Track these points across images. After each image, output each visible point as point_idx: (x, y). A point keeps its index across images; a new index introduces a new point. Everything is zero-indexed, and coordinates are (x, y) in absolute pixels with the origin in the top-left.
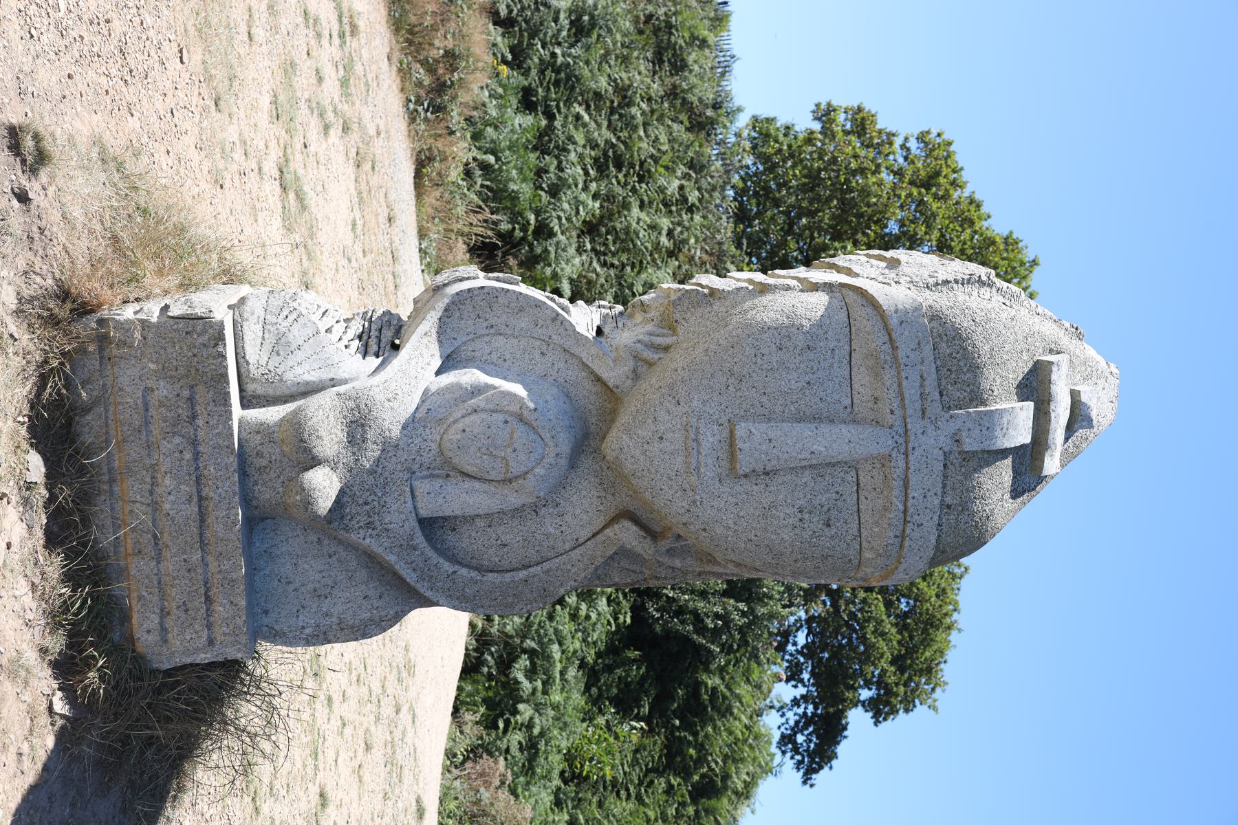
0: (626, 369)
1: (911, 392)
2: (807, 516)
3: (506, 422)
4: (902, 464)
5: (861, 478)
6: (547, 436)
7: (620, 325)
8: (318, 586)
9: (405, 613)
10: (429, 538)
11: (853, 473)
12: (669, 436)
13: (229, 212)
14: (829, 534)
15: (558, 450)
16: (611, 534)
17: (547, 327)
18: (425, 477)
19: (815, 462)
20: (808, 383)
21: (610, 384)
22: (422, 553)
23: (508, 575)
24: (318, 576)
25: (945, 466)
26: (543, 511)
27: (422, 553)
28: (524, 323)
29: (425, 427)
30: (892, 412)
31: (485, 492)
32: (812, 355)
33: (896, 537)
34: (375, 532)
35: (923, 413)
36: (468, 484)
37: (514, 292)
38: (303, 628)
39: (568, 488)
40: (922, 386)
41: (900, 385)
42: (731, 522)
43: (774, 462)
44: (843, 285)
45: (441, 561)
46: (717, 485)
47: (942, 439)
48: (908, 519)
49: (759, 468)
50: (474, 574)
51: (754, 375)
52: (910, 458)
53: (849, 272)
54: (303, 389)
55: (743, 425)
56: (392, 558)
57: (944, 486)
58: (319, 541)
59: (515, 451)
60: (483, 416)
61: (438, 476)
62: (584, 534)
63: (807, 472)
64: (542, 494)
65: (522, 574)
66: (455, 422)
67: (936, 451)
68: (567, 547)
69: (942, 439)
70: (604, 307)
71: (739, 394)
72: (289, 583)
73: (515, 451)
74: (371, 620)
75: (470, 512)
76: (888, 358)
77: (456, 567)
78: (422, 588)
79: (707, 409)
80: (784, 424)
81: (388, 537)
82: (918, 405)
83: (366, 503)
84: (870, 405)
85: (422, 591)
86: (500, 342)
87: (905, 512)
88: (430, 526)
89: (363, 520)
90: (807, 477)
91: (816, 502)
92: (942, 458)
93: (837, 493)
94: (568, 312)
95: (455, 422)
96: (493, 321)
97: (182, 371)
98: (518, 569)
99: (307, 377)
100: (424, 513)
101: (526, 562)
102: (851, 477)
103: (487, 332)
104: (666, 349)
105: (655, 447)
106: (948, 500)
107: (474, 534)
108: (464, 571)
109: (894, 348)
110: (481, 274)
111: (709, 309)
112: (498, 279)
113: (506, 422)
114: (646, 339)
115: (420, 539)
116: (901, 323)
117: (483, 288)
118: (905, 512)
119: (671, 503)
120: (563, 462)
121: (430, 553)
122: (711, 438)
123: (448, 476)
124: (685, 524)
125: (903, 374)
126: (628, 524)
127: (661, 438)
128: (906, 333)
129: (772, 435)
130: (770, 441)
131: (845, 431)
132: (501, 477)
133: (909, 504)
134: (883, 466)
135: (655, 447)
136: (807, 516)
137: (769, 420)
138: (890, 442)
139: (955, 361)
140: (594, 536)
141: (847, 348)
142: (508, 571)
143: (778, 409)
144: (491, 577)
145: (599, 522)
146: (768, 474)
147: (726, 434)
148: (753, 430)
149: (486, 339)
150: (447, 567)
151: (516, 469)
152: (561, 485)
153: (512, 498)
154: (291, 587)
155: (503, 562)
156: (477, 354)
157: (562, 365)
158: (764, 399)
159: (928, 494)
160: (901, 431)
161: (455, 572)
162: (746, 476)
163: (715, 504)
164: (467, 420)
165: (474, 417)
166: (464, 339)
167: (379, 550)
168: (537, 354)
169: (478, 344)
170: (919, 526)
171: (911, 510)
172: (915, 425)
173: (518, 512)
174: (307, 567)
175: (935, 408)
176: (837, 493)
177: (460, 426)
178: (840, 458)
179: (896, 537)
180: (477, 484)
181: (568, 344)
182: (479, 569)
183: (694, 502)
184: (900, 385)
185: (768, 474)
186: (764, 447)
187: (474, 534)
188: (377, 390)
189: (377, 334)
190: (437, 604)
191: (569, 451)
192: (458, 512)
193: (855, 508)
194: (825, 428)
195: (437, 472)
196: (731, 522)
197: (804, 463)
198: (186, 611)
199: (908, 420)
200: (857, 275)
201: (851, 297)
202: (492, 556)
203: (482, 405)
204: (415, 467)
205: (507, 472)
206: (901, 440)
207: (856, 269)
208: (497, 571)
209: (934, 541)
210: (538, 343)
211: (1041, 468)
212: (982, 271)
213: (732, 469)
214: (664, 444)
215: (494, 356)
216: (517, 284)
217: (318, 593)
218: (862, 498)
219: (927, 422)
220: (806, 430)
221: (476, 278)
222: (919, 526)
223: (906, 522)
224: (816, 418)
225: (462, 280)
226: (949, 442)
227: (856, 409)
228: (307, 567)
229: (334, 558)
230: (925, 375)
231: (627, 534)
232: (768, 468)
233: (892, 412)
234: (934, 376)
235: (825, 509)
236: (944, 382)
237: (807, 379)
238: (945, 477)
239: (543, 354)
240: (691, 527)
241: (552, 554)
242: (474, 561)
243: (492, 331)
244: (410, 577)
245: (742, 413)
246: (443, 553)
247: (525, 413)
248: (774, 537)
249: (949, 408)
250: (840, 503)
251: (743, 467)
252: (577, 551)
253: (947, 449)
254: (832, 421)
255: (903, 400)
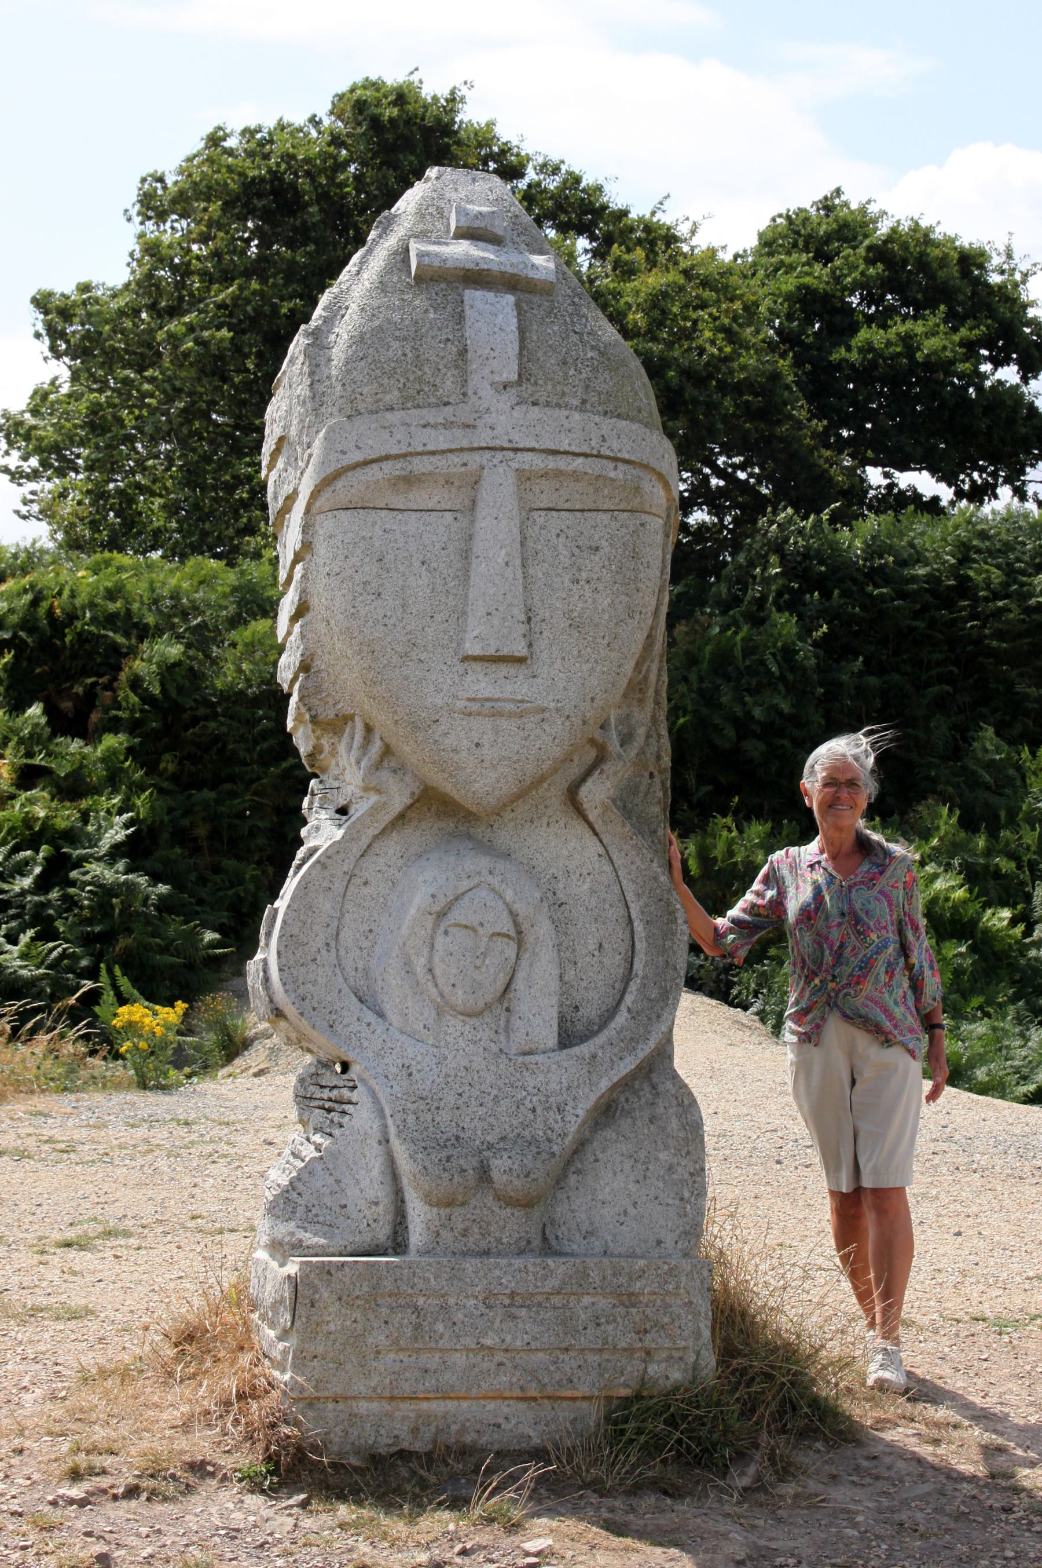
0: (391, 781)
1: (441, 440)
2: (584, 575)
3: (446, 933)
4: (528, 456)
5: (542, 506)
6: (466, 884)
7: (336, 784)
8: (632, 1178)
9: (675, 1076)
10: (584, 1038)
11: (535, 515)
12: (475, 736)
13: (144, 1291)
14: (607, 549)
15: (485, 872)
16: (596, 812)
17: (332, 876)
18: (508, 1037)
19: (518, 562)
20: (423, 563)
21: (409, 801)
22: (602, 1047)
23: (638, 946)
24: (621, 1177)
25: (534, 404)
26: (561, 896)
27: (602, 1047)
28: (326, 906)
29: (446, 1033)
30: (465, 465)
31: (531, 965)
32: (390, 557)
33: (616, 468)
34: (571, 1103)
35: (468, 426)
36: (519, 984)
37: (286, 914)
38: (682, 1199)
39: (534, 863)
40: (434, 426)
41: (433, 453)
42: (585, 667)
43: (515, 611)
44: (307, 511)
45: (613, 1025)
46: (539, 680)
47: (501, 405)
48: (595, 452)
49: (523, 628)
50: (633, 986)
51: (409, 628)
52: (521, 446)
53: (291, 498)
54: (389, 1179)
55: (467, 645)
56: (605, 1084)
57: (558, 406)
58: (578, 1172)
59: (482, 924)
60: (437, 959)
61: (508, 1021)
62: (593, 847)
63: (531, 571)
64: (538, 895)
65: (638, 926)
66: (442, 995)
67: (515, 414)
68: (607, 868)
69: (501, 405)
70: (311, 803)
71: (430, 648)
72: (625, 1212)
73: (482, 924)
74: (679, 1117)
75: (554, 986)
76: (399, 466)
77: (623, 1007)
78: (645, 1050)
79: (445, 687)
80: (471, 596)
81: (578, 1086)
82: (459, 433)
83: (534, 1110)
84: (454, 490)
85: (648, 1051)
86: (346, 935)
87: (586, 455)
88: (567, 1038)
89: (553, 1116)
90: (536, 571)
91: (567, 561)
92: (524, 407)
93: (558, 535)
94: (315, 850)
95: (442, 995)
96: (320, 942)
97: (357, 1314)
98: (632, 932)
99: (376, 1172)
100: (552, 1041)
101: (623, 921)
102: (540, 517)
103: (333, 951)
104: (369, 729)
105: (486, 752)
106: (575, 402)
107: (584, 984)
108: (629, 999)
109: (387, 458)
110: (259, 956)
111: (324, 674)
112: (269, 934)
113: (446, 933)
114: (355, 753)
115: (584, 1050)
116: (358, 447)
117: (279, 953)
118: (586, 455)
119: (548, 742)
120: (501, 866)
121: (601, 1038)
122: (482, 684)
123: (508, 1010)
124: (584, 723)
125: (420, 449)
126: (584, 792)
127: (477, 745)
128: (370, 442)
129: (481, 611)
130: (489, 614)
131: (484, 522)
132: (514, 946)
133: (578, 450)
134: (529, 479)
135: (486, 752)
136: (584, 575)
137: (464, 613)
138: (501, 470)
139: (408, 385)
140: (596, 834)
141: (383, 513)
142: (633, 945)
143: (451, 601)
144: (638, 966)
145: (580, 827)
146: (529, 619)
147: (477, 666)
148: (475, 633)
149: (342, 952)
150: (621, 1018)
151: (505, 925)
152: (531, 871)
153: (542, 931)
154: (632, 1211)
155: (622, 950)
156: (360, 966)
157: (381, 860)
158: (438, 618)
159: (567, 425)
160: (488, 454)
161: (629, 1010)
162: (530, 645)
163: (561, 684)
164: (441, 981)
165: (438, 972)
166: (341, 980)
167: (593, 1098)
168: (366, 891)
169: (348, 964)
170: (604, 440)
171: (585, 449)
172: (483, 438)
173: (560, 926)
174: (608, 1189)
175: (464, 413)
176: (558, 535)
177: (447, 990)
178: (516, 531)
179: (616, 468)
180: (520, 975)
181: (356, 850)
182: (628, 978)
183: (558, 710)
184: (433, 453)
185: (529, 619)
186: (496, 622)
187: (584, 984)
188: (396, 1088)
189: (327, 1090)
190: (668, 1039)
191: (488, 858)
192: (554, 1000)
193: (578, 514)
194: (478, 547)
195: (502, 1023)
196: (585, 667)
197: (519, 574)
198: (646, 1331)
199: (476, 445)
200: (295, 493)
201: (321, 503)
202: (615, 962)
203: (423, 961)
204: (494, 1048)
205: (508, 936)
206: (499, 456)
207: (287, 489)
208: (633, 958)
209: (624, 423)
210: (351, 888)
211: (545, 282)
212: (298, 344)
213: (521, 660)
214: (486, 741)
215: (365, 944)
216: (276, 910)
217: (641, 1178)
218: (566, 506)
219: (480, 423)
220: (479, 569)
221: (265, 962)
222: (604, 440)
223: (599, 456)
224: (466, 555)
225: (267, 979)
226: (505, 397)
227: (458, 507)
228: (608, 1189)
229: (600, 1156)
230: (422, 422)
231: (596, 793)
232: (523, 617)
233: (465, 465)
234: (425, 411)
235: (576, 551)
236: (433, 400)
237: (417, 564)
238: (548, 404)
239: (366, 883)
240: (588, 715)
241: (616, 889)
242: (617, 985)
243: (333, 944)
244: (629, 1064)
245: (454, 645)
246: (604, 1023)
247: (436, 908)
248: (606, 616)
249: (464, 394)
250: (571, 533)
251: (519, 649)
252: (614, 857)
253: (514, 400)
254: (471, 537)
255: (451, 451)
